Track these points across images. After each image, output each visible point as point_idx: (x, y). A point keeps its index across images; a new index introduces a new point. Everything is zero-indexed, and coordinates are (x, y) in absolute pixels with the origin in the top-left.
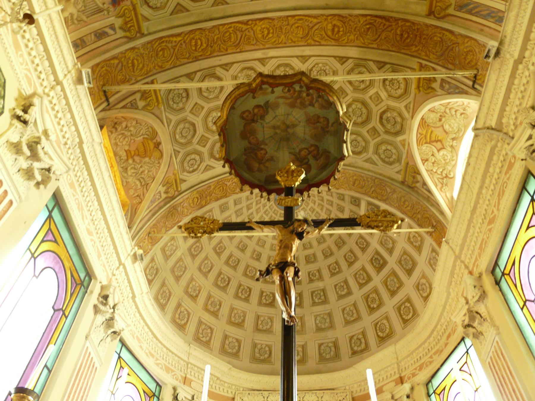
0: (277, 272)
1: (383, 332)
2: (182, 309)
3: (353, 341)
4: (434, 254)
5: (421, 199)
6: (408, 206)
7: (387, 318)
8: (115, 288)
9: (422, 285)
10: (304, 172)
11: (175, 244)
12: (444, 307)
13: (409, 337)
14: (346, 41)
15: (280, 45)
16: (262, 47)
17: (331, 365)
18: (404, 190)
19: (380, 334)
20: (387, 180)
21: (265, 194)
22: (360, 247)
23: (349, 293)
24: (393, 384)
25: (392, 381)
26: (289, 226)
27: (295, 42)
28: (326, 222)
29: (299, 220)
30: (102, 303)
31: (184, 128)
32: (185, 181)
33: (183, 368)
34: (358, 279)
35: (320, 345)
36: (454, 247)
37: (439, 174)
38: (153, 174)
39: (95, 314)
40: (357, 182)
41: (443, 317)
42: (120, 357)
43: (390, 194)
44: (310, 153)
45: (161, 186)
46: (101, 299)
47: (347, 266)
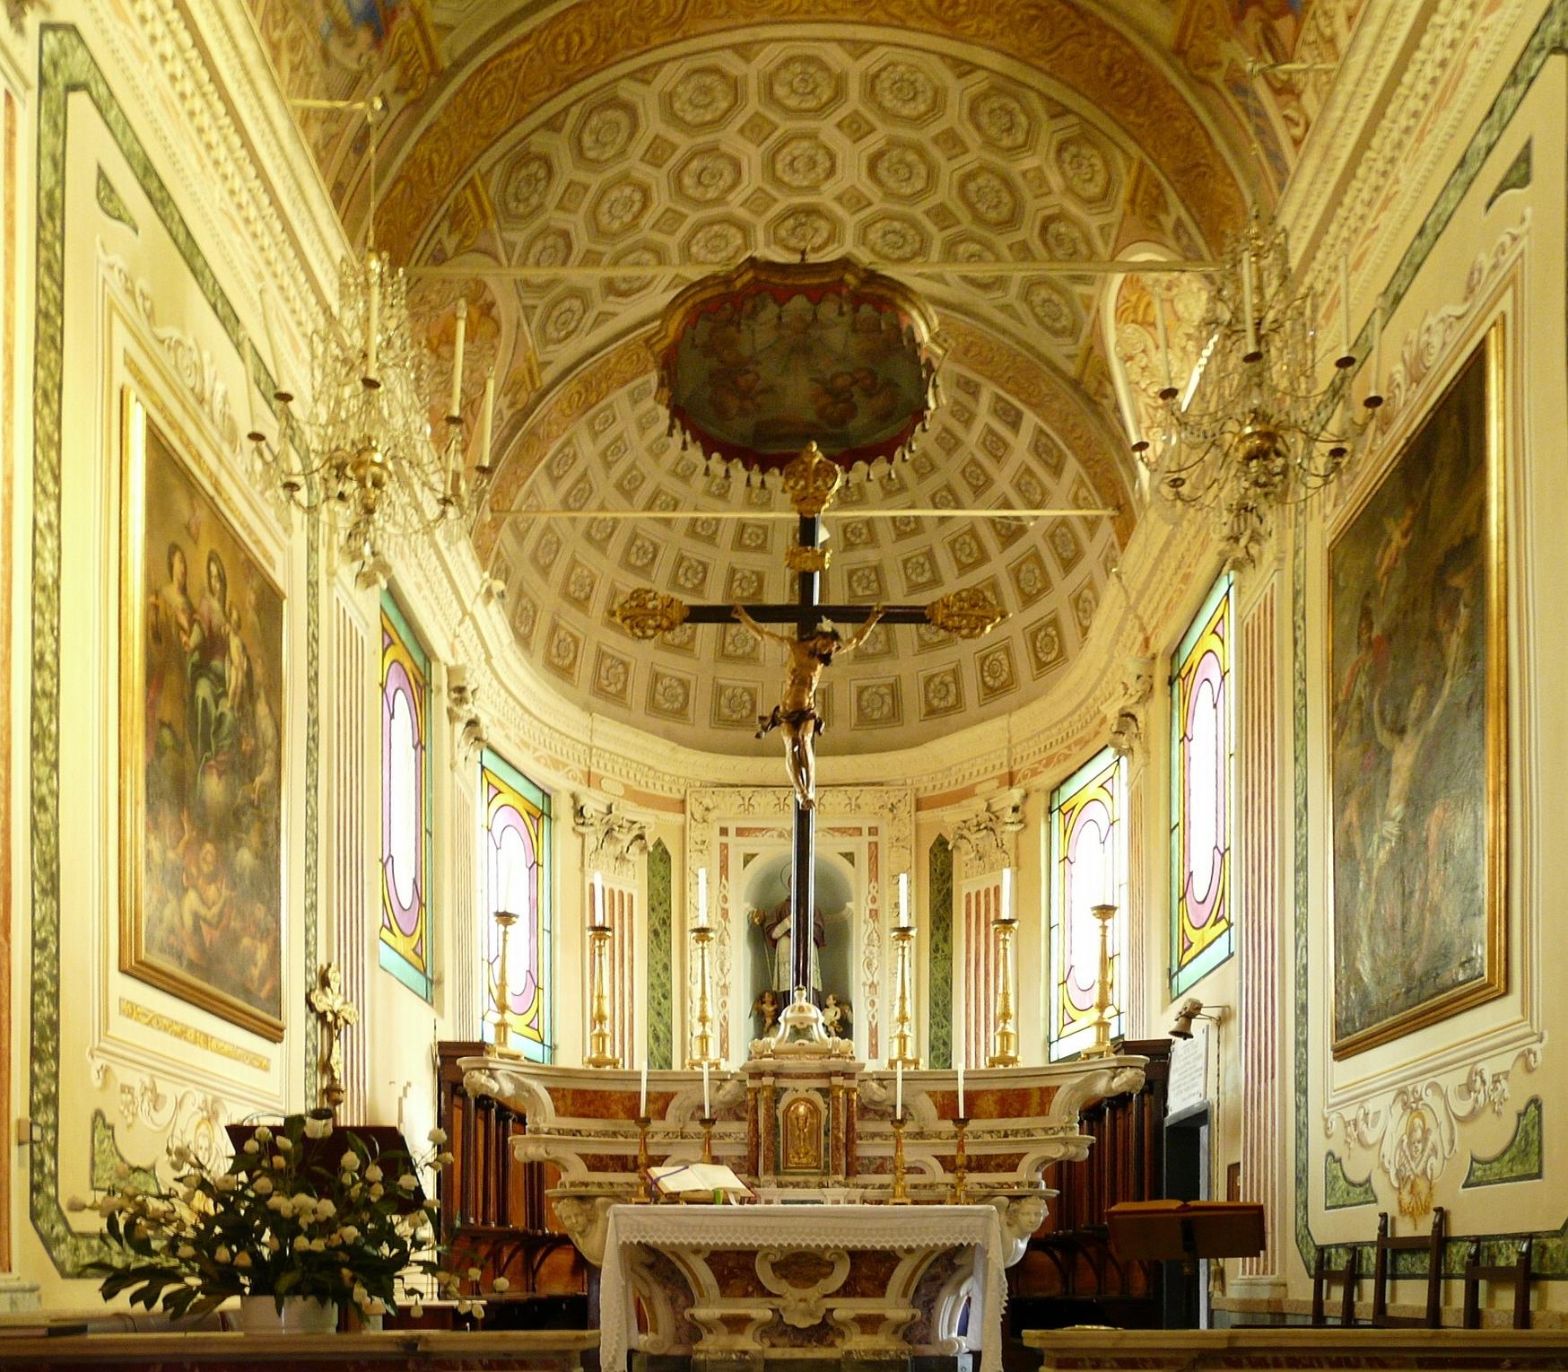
7: (1007, 650)
14: (972, 30)
15: (795, 17)
16: (742, 21)
17: (881, 734)
24: (995, 783)
27: (834, 12)
31: (544, 248)
35: (861, 691)
40: (974, 351)
42: (483, 768)
44: (855, 382)
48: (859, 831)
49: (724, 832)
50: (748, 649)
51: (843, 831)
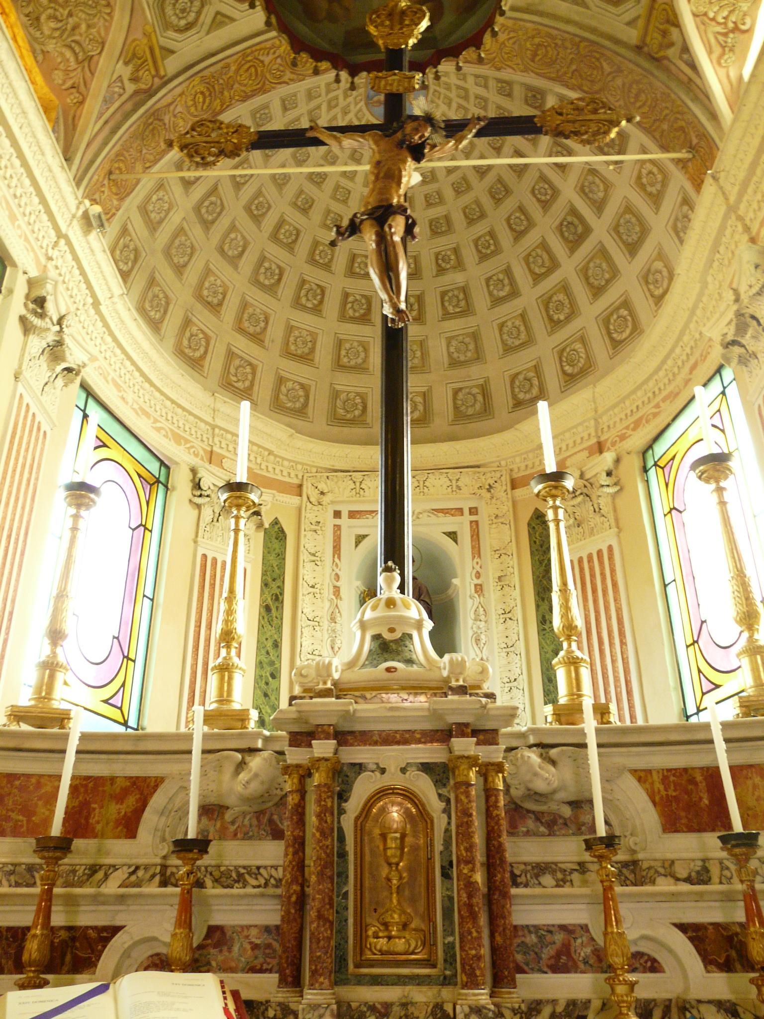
0: (372, 225)
1: (573, 366)
2: (194, 329)
3: (517, 383)
4: (685, 208)
5: (673, 85)
6: (644, 104)
7: (583, 340)
8: (56, 282)
9: (653, 274)
10: (428, 14)
11: (166, 198)
12: (693, 312)
13: (621, 371)
18: (638, 65)
19: (568, 368)
20: (607, 43)
21: (344, 75)
22: (539, 200)
23: (514, 293)
24: (586, 453)
25: (582, 450)
26: (395, 132)
28: (470, 126)
29: (416, 118)
30: (35, 313)
32: (172, 52)
33: (205, 436)
34: (532, 266)
35: (456, 392)
36: (727, 187)
37: (719, 24)
38: (99, 32)
39: (25, 335)
41: (688, 331)
43: (610, 78)
45: (121, 62)
46: (31, 306)
47: (512, 239)
48: (460, 511)
49: (337, 514)
50: (360, 361)
51: (445, 511)
